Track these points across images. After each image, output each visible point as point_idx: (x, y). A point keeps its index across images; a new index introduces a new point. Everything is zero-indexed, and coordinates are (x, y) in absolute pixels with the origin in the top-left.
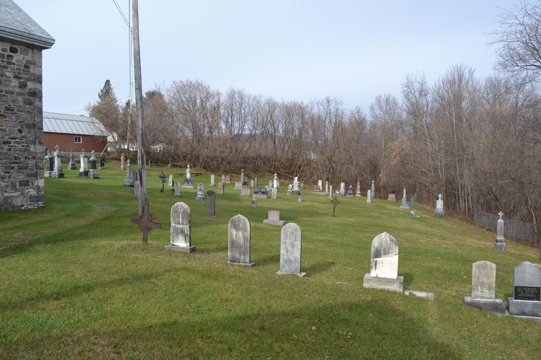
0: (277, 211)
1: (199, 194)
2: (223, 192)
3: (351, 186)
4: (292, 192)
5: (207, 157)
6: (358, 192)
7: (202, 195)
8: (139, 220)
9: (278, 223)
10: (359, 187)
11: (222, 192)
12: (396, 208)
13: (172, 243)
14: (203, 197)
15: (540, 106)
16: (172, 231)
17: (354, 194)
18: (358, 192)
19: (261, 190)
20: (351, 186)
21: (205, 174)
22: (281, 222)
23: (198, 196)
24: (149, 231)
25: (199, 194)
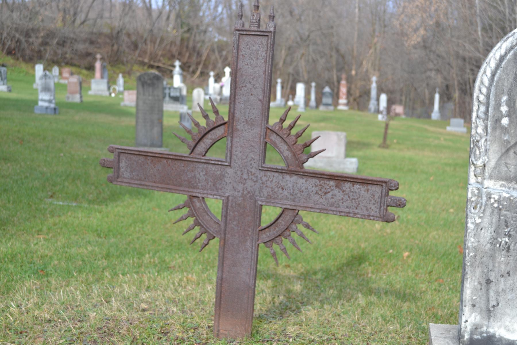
0: (339, 133)
1: (43, 100)
2: (81, 97)
3: (327, 89)
4: (221, 99)
5: (17, 30)
6: (343, 101)
7: (50, 101)
8: (178, 159)
9: (342, 166)
10: (343, 90)
11: (77, 98)
12: (441, 130)
13: (476, 328)
14: (52, 106)
15: (391, 4)
16: (487, 235)
17: (336, 104)
18: (343, 101)
19: (169, 94)
20: (327, 89)
21: (12, 66)
22: (351, 163)
23: (41, 103)
24: (268, 243)
25: (43, 100)
